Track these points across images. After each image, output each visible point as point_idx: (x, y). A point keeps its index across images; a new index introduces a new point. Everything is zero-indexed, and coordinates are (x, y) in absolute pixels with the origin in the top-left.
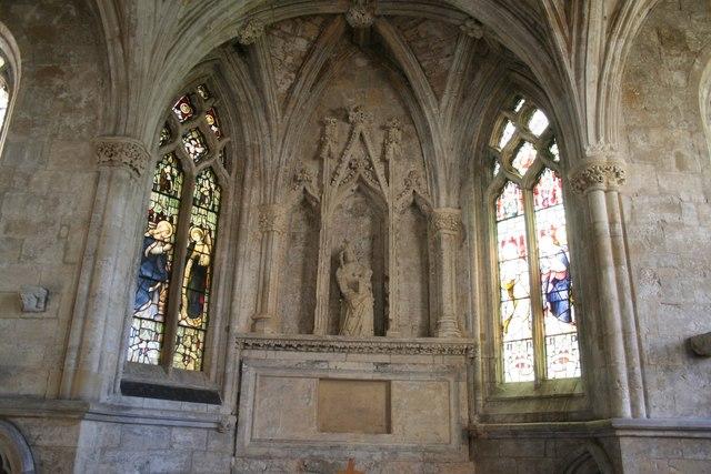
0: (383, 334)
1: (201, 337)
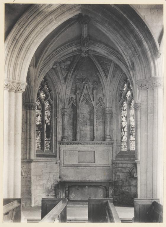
0: (93, 140)
1: (50, 142)
